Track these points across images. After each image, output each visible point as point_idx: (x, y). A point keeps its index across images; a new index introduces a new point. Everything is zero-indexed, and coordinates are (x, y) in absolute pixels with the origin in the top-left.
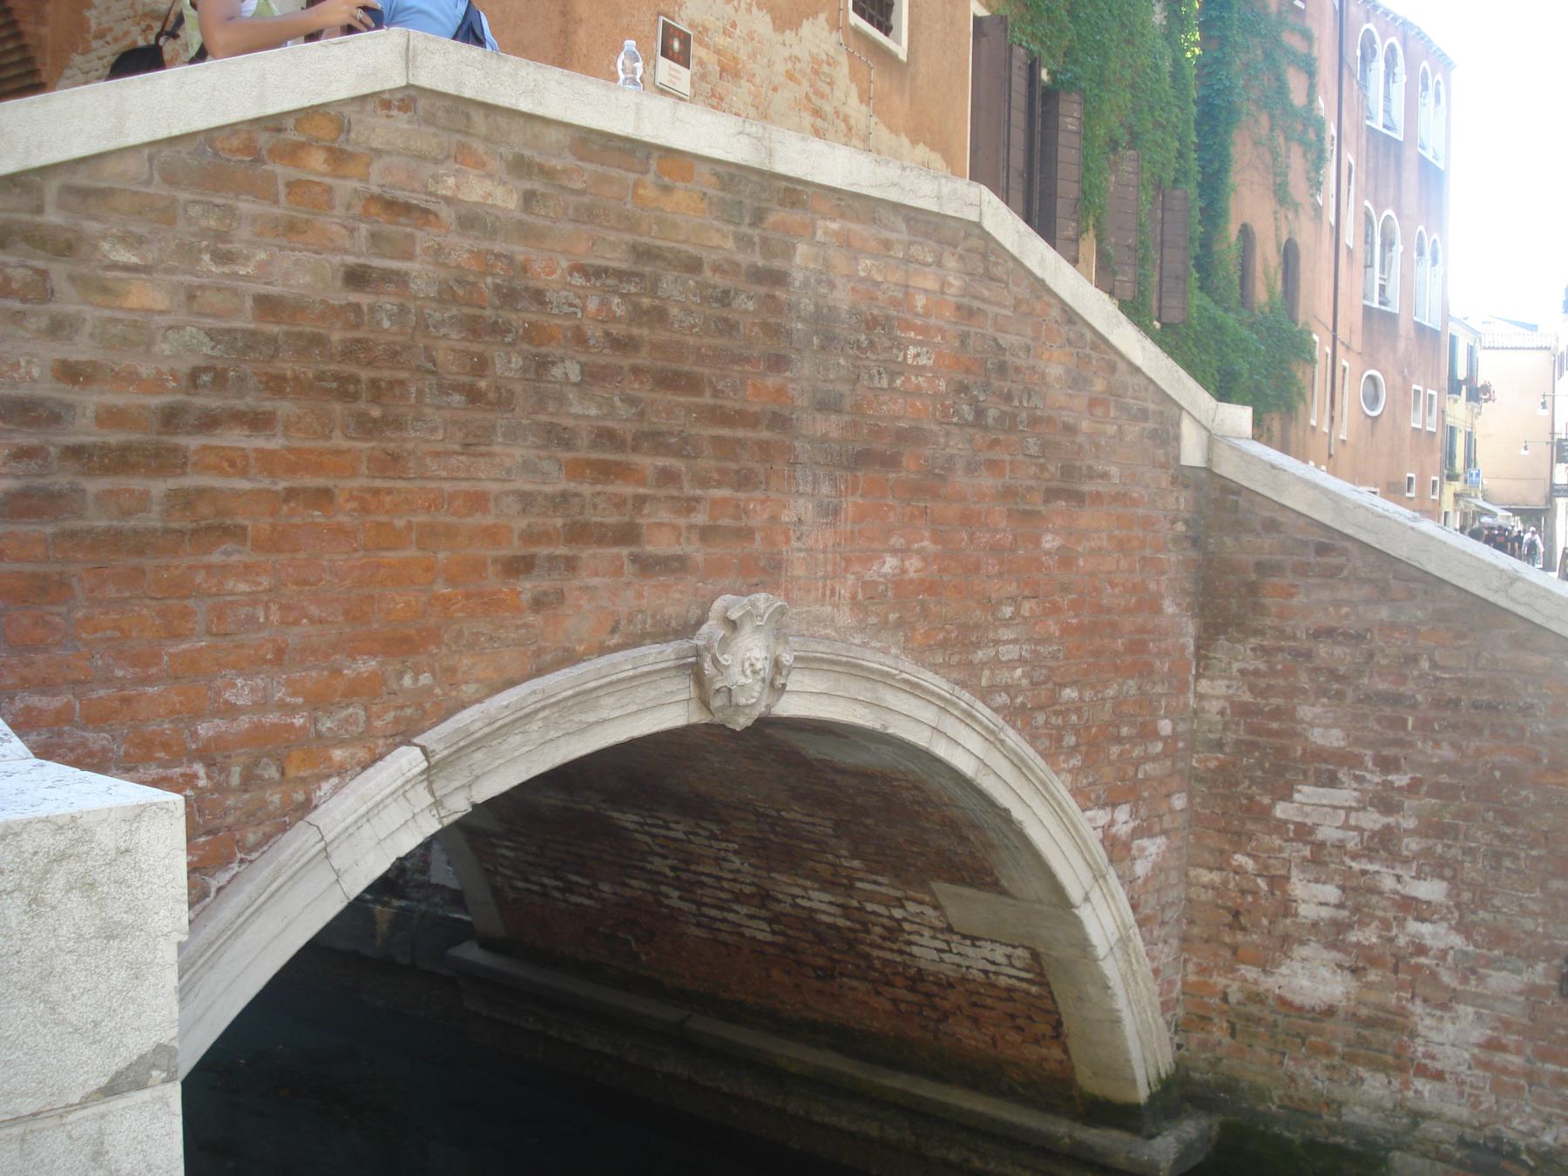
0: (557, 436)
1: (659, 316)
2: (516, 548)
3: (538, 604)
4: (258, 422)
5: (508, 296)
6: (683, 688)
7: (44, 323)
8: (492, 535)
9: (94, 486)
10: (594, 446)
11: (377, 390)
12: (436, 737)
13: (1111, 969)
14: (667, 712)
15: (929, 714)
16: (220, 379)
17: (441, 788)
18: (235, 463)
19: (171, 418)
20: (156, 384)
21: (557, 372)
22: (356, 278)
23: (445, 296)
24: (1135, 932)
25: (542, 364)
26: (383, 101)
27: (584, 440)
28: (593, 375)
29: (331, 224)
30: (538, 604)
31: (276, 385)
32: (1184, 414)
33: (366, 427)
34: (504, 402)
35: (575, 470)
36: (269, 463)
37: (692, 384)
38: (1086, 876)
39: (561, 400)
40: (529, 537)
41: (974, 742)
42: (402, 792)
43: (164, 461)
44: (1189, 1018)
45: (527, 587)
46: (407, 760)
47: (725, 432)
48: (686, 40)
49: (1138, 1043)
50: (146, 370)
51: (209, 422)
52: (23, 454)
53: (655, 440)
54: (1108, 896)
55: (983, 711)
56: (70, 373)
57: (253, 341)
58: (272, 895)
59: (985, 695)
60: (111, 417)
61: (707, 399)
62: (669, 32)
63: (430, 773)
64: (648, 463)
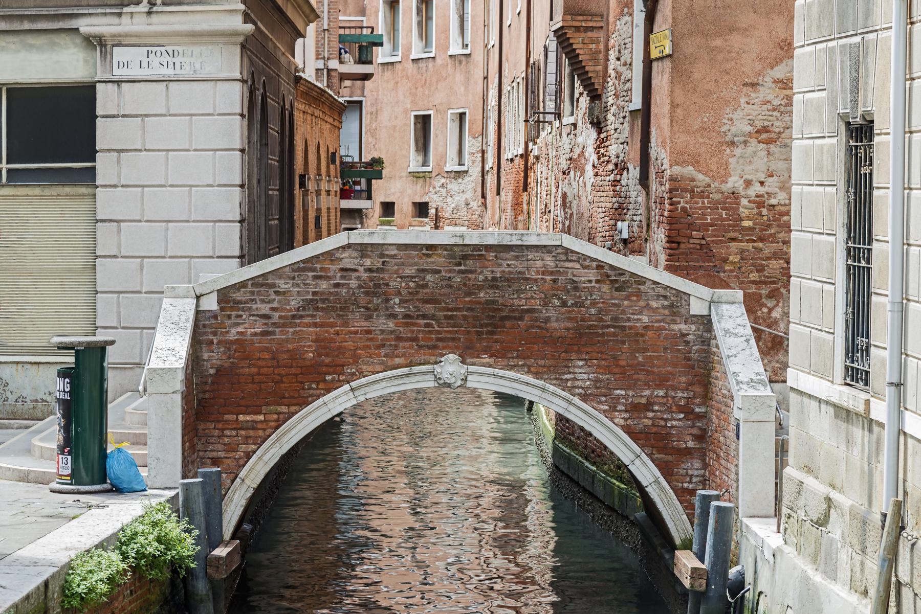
1: (426, 286)
2: (380, 343)
3: (386, 356)
6: (431, 377)
7: (378, 209)
10: (403, 318)
12: (354, 384)
16: (304, 308)
17: (356, 393)
18: (308, 325)
19: (294, 317)
20: (291, 310)
21: (392, 302)
22: (337, 285)
23: (360, 287)
25: (387, 300)
26: (343, 248)
27: (400, 316)
31: (317, 309)
32: (692, 298)
39: (393, 308)
40: (382, 340)
42: (345, 393)
46: (346, 387)
47: (450, 313)
49: (673, 524)
50: (288, 308)
51: (301, 317)
52: (266, 324)
53: (424, 317)
56: (272, 309)
57: (311, 300)
58: (125, 368)
59: (570, 390)
60: (280, 317)
64: (422, 322)
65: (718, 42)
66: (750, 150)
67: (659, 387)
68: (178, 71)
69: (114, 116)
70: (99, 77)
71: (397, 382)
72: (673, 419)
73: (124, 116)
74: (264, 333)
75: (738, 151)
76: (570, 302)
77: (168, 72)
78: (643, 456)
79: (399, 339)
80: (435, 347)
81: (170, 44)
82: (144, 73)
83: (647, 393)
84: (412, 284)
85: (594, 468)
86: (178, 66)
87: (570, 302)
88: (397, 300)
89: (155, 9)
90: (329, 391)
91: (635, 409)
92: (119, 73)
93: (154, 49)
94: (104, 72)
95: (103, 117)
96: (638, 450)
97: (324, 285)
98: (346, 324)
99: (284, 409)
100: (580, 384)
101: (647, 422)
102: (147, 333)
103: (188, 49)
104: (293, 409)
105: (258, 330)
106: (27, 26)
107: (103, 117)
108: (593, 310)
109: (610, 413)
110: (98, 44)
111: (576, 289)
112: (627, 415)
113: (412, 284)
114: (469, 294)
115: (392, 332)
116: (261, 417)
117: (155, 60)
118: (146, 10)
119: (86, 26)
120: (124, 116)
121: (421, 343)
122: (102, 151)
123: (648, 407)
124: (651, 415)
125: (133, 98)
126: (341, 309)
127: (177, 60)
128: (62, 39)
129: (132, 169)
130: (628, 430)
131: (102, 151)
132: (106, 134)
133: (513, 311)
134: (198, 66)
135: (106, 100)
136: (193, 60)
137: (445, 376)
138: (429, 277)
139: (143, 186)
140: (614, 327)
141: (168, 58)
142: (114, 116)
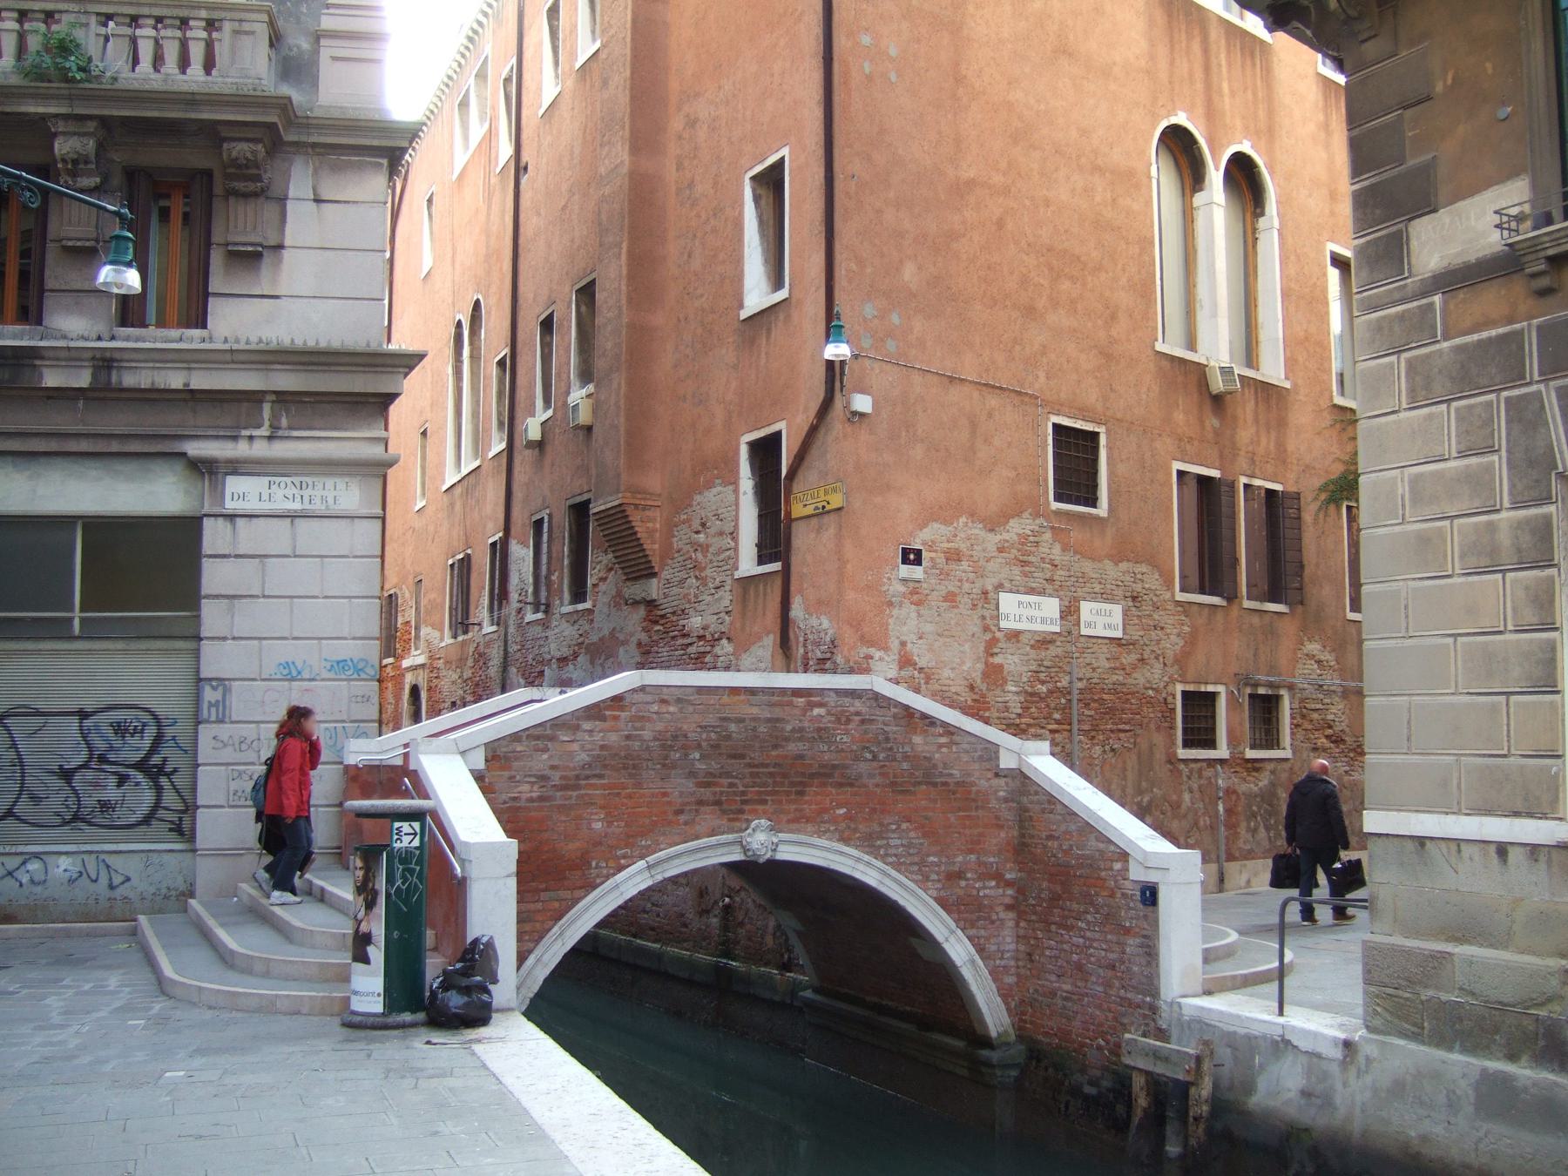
0: (692, 774)
1: (728, 737)
3: (686, 823)
4: (600, 776)
5: (675, 737)
6: (738, 849)
8: (669, 803)
9: (559, 794)
11: (635, 767)
13: (967, 973)
14: (940, 938)
15: (850, 862)
19: (577, 777)
20: (574, 769)
22: (628, 737)
24: (977, 957)
28: (703, 757)
29: (621, 724)
30: (686, 823)
31: (605, 766)
33: (631, 776)
34: (674, 767)
35: (699, 785)
36: (604, 787)
37: (742, 756)
38: (946, 933)
41: (874, 873)
42: (640, 872)
43: (577, 787)
44: (1020, 1006)
45: (682, 818)
46: (641, 864)
48: (918, 553)
51: (587, 778)
53: (728, 775)
54: (959, 940)
55: (879, 864)
59: (883, 858)
61: (748, 760)
62: (906, 552)
63: (649, 867)
64: (725, 781)
65: (878, 500)
66: (904, 611)
67: (971, 851)
68: (307, 506)
69: (224, 556)
70: (206, 510)
71: (700, 855)
72: (985, 888)
73: (237, 556)
74: (541, 799)
75: (895, 612)
76: (882, 756)
77: (296, 506)
78: (959, 932)
79: (700, 803)
80: (741, 812)
81: (296, 475)
82: (265, 507)
83: (960, 859)
84: (713, 735)
85: (657, 946)
86: (306, 499)
87: (882, 756)
88: (697, 756)
89: (280, 433)
90: (621, 869)
91: (954, 876)
92: (231, 505)
93: (278, 479)
94: (212, 505)
95: (211, 556)
96: (953, 925)
97: (613, 738)
98: (638, 785)
99: (566, 894)
100: (893, 851)
101: (961, 892)
102: (1517, 704)
103: (319, 481)
104: (577, 893)
105: (534, 795)
106: (115, 447)
107: (211, 556)
108: (905, 766)
109: (923, 882)
110: (207, 471)
111: (887, 740)
112: (939, 885)
113: (713, 735)
114: (775, 747)
115: (692, 794)
116: (539, 906)
117: (279, 493)
118: (267, 434)
119: (195, 449)
120: (237, 556)
121: (725, 807)
122: (208, 597)
123: (960, 875)
124: (963, 883)
125: (249, 536)
126: (635, 767)
127: (306, 493)
128: (158, 466)
129: (247, 619)
130: (943, 903)
131: (208, 597)
132: (214, 577)
133: (824, 766)
134: (331, 501)
135: (214, 536)
136: (325, 493)
137: (755, 846)
138: (733, 727)
139: (260, 639)
140: (928, 783)
141: (295, 491)
142: (224, 556)
